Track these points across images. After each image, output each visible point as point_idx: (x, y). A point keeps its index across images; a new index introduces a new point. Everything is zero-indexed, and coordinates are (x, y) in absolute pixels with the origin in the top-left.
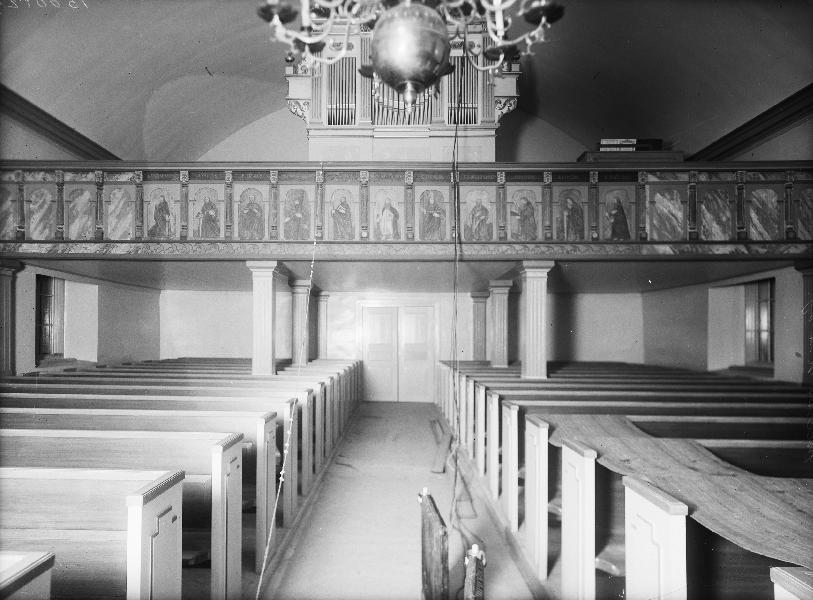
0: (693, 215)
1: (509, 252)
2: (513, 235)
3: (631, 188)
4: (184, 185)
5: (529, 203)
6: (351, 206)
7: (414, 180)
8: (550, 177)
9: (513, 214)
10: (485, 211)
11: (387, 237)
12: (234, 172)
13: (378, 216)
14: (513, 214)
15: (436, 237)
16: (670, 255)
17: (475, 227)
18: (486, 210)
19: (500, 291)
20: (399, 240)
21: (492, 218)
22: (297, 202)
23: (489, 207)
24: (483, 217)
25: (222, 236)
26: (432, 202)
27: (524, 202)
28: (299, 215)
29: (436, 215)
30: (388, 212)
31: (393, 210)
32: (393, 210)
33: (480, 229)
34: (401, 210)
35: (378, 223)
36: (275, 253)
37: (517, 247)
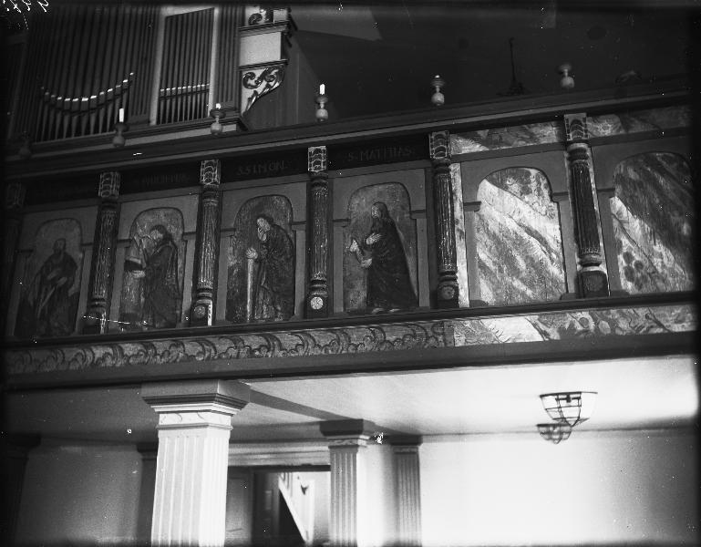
24: (63, 280)
27: (158, 235)
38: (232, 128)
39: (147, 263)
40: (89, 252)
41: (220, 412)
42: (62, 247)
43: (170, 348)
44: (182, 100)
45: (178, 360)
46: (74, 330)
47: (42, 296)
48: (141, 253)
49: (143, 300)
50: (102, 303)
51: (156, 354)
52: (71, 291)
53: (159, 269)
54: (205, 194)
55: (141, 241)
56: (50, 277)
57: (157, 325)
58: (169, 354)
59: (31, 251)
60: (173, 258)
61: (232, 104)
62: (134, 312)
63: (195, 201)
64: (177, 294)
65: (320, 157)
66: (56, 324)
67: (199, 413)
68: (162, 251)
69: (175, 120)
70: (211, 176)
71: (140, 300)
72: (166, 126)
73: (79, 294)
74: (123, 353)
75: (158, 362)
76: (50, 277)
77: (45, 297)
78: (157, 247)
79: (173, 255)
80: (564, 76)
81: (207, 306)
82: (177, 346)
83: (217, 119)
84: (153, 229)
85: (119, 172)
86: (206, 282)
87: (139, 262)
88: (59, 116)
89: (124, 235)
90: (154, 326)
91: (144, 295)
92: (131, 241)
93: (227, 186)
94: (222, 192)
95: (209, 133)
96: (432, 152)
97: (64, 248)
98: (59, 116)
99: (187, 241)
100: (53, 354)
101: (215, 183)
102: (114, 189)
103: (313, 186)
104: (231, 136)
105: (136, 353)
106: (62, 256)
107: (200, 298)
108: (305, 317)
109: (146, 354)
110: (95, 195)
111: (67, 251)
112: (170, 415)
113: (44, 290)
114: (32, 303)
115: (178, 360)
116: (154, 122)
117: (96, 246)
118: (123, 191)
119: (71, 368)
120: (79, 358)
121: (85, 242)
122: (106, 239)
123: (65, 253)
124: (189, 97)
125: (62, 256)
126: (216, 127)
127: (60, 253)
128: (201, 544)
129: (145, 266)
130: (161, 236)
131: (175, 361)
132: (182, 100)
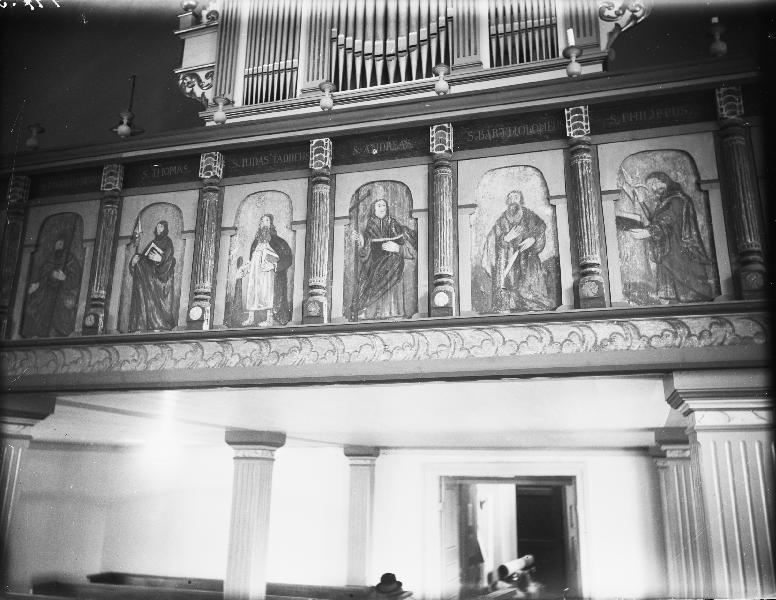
1: (620, 344)
2: (629, 289)
4: (205, 189)
5: (673, 188)
6: (178, 245)
7: (334, 163)
8: (449, 139)
9: (624, 224)
10: (533, 223)
11: (260, 316)
12: (338, 140)
13: (240, 262)
14: (624, 224)
15: (389, 311)
16: (19, 350)
17: (506, 272)
18: (539, 221)
19: (362, 462)
20: (175, 331)
21: (557, 243)
22: (59, 245)
23: (544, 212)
24: (528, 243)
25: (15, 337)
26: (380, 212)
27: (659, 185)
28: (60, 275)
29: (391, 247)
30: (264, 248)
31: (277, 243)
32: (277, 243)
33: (520, 277)
34: (296, 241)
35: (239, 281)
36: (360, 358)
37: (648, 327)
38: (598, 68)
39: (650, 219)
40: (301, 232)
41: (707, 410)
42: (518, 201)
43: (711, 326)
44: (273, 78)
45: (715, 344)
46: (560, 303)
47: (503, 261)
48: (638, 206)
49: (653, 266)
50: (320, 291)
51: (690, 335)
52: (544, 256)
53: (670, 227)
54: (314, 179)
55: (634, 193)
56: (508, 238)
57: (682, 298)
58: (711, 334)
59: (474, 206)
60: (688, 212)
61: (590, 40)
62: (644, 281)
63: (194, 195)
64: (704, 259)
65: (580, 111)
66: (530, 297)
67: (728, 413)
68: (668, 204)
69: (278, 98)
70: (321, 158)
71: (648, 265)
72: (503, 69)
73: (557, 259)
74: (638, 333)
75: (696, 345)
76: (508, 238)
77: (507, 263)
78: (661, 200)
79: (688, 208)
80: (714, 40)
81: (321, 305)
82: (721, 325)
83: (574, 59)
84: (649, 177)
85: (332, 139)
86: (446, 268)
87: (638, 218)
88: (359, 61)
89: (227, 222)
90: (678, 300)
91: (655, 261)
92: (133, 238)
93: (461, 154)
94: (333, 176)
95: (566, 76)
96: (721, 103)
97: (522, 202)
98: (359, 61)
99: (295, 231)
100: (536, 333)
101: (327, 167)
102: (218, 169)
103: (573, 153)
104: (504, 91)
105: (659, 333)
106: (521, 212)
107: (312, 295)
108: (577, 305)
109: (675, 335)
110: (96, 188)
111: (526, 206)
112: (709, 413)
113: (502, 255)
114: (489, 271)
115: (726, 343)
116: (486, 65)
117: (198, 232)
118: (337, 161)
119: (564, 350)
120: (575, 339)
121: (185, 229)
122: (210, 225)
123: (525, 209)
124: (530, 34)
125: (521, 212)
126: (575, 67)
127: (517, 209)
128: (251, 597)
129: (647, 223)
130: (664, 185)
131: (722, 344)
132: (273, 78)
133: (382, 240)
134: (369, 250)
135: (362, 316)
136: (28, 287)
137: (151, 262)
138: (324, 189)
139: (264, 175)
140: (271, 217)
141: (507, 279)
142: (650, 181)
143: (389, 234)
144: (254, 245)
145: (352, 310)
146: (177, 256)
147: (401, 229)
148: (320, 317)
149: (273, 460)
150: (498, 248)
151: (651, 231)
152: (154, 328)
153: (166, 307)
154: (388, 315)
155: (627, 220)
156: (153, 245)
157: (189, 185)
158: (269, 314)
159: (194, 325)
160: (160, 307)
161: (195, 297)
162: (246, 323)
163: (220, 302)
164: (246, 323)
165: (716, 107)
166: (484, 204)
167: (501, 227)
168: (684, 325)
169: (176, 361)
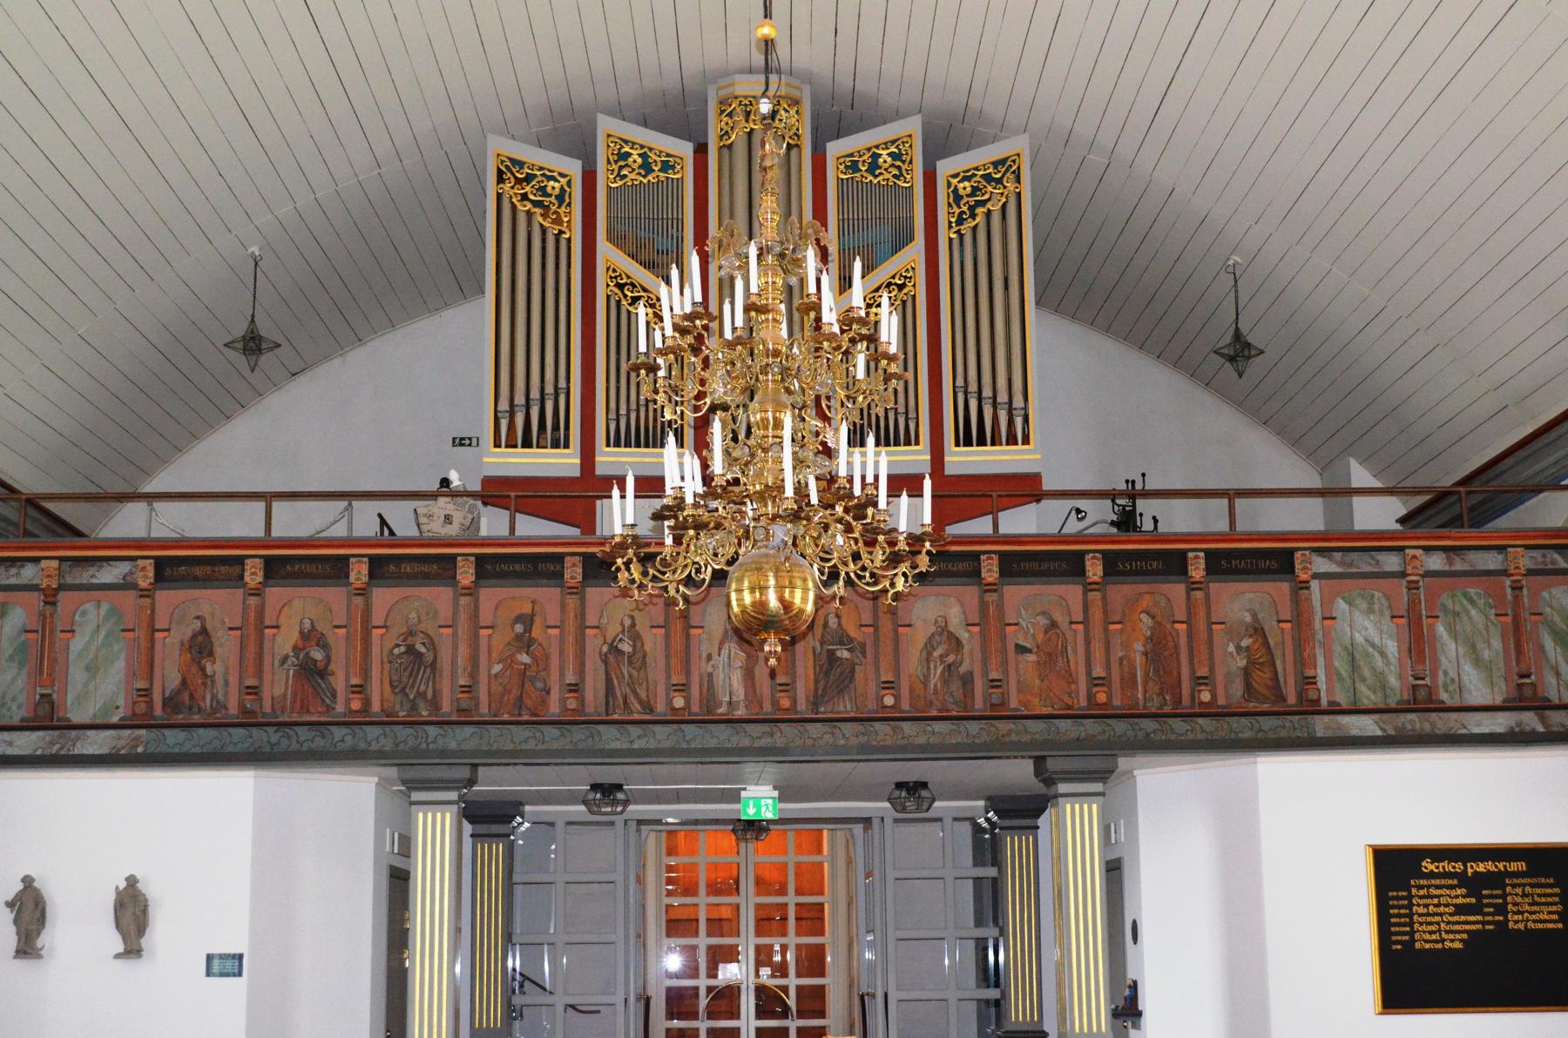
0: (1418, 645)
3: (1280, 589)
8: (365, 569)
12: (269, 562)
13: (709, 657)
14: (1021, 650)
23: (964, 635)
24: (951, 658)
29: (844, 654)
35: (710, 675)
42: (943, 624)
47: (932, 672)
52: (963, 669)
54: (1192, 586)
76: (936, 654)
87: (1029, 646)
127: (943, 630)
129: (1035, 650)
133: (835, 647)
134: (824, 655)
135: (822, 709)
136: (490, 668)
137: (621, 653)
138: (1198, 595)
139: (526, 582)
140: (1044, 613)
141: (935, 685)
142: (1038, 618)
143: (841, 643)
144: (721, 643)
145: (815, 704)
146: (648, 647)
147: (851, 640)
148: (1318, 701)
149: (1038, 828)
150: (928, 661)
151: (1037, 656)
152: (632, 712)
153: (643, 694)
154: (842, 708)
155: (1022, 647)
156: (621, 636)
157: (1077, 579)
158: (742, 704)
159: (888, 710)
160: (635, 692)
161: (1199, 681)
162: (720, 711)
163: (695, 691)
164: (720, 711)
165: (1187, 568)
166: (918, 624)
167: (929, 647)
168: (994, 726)
169: (659, 742)
